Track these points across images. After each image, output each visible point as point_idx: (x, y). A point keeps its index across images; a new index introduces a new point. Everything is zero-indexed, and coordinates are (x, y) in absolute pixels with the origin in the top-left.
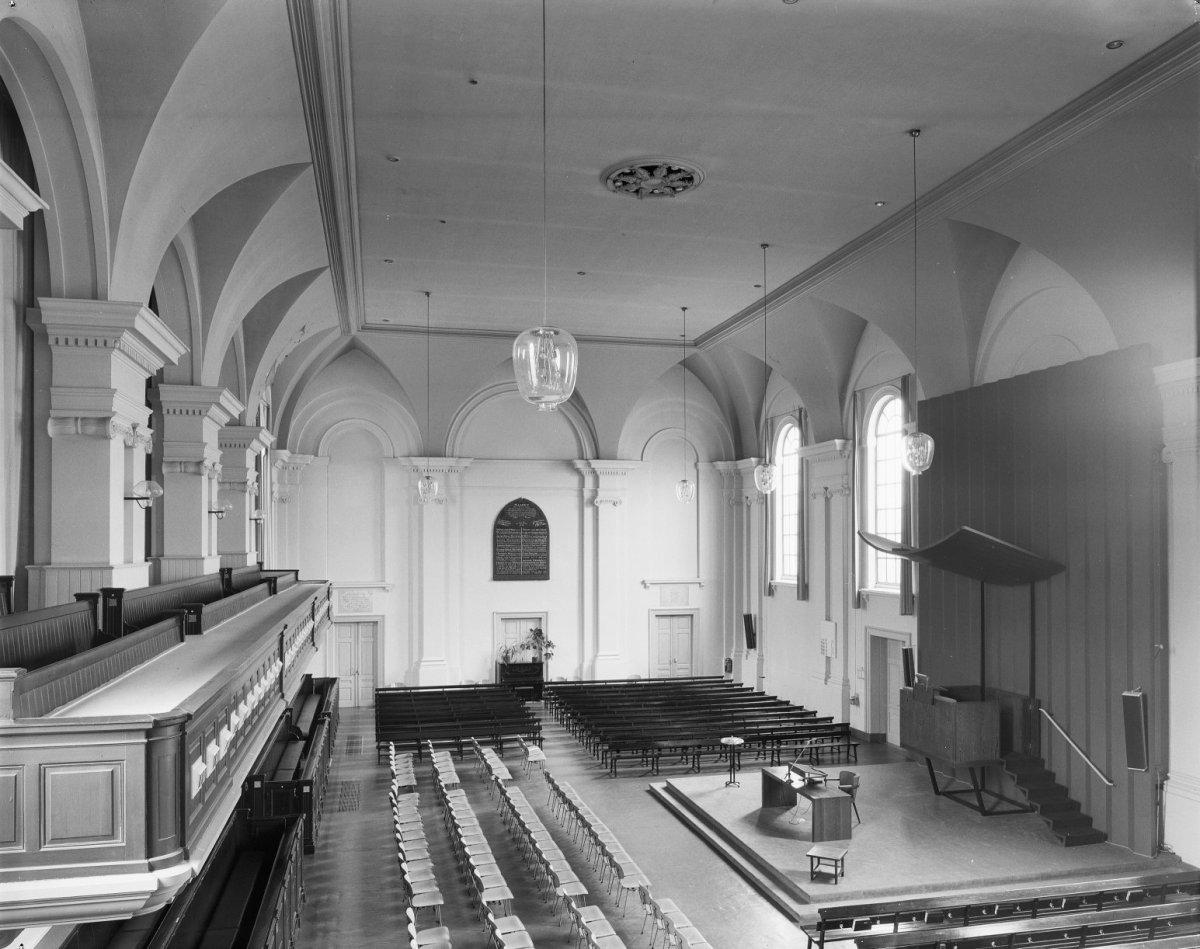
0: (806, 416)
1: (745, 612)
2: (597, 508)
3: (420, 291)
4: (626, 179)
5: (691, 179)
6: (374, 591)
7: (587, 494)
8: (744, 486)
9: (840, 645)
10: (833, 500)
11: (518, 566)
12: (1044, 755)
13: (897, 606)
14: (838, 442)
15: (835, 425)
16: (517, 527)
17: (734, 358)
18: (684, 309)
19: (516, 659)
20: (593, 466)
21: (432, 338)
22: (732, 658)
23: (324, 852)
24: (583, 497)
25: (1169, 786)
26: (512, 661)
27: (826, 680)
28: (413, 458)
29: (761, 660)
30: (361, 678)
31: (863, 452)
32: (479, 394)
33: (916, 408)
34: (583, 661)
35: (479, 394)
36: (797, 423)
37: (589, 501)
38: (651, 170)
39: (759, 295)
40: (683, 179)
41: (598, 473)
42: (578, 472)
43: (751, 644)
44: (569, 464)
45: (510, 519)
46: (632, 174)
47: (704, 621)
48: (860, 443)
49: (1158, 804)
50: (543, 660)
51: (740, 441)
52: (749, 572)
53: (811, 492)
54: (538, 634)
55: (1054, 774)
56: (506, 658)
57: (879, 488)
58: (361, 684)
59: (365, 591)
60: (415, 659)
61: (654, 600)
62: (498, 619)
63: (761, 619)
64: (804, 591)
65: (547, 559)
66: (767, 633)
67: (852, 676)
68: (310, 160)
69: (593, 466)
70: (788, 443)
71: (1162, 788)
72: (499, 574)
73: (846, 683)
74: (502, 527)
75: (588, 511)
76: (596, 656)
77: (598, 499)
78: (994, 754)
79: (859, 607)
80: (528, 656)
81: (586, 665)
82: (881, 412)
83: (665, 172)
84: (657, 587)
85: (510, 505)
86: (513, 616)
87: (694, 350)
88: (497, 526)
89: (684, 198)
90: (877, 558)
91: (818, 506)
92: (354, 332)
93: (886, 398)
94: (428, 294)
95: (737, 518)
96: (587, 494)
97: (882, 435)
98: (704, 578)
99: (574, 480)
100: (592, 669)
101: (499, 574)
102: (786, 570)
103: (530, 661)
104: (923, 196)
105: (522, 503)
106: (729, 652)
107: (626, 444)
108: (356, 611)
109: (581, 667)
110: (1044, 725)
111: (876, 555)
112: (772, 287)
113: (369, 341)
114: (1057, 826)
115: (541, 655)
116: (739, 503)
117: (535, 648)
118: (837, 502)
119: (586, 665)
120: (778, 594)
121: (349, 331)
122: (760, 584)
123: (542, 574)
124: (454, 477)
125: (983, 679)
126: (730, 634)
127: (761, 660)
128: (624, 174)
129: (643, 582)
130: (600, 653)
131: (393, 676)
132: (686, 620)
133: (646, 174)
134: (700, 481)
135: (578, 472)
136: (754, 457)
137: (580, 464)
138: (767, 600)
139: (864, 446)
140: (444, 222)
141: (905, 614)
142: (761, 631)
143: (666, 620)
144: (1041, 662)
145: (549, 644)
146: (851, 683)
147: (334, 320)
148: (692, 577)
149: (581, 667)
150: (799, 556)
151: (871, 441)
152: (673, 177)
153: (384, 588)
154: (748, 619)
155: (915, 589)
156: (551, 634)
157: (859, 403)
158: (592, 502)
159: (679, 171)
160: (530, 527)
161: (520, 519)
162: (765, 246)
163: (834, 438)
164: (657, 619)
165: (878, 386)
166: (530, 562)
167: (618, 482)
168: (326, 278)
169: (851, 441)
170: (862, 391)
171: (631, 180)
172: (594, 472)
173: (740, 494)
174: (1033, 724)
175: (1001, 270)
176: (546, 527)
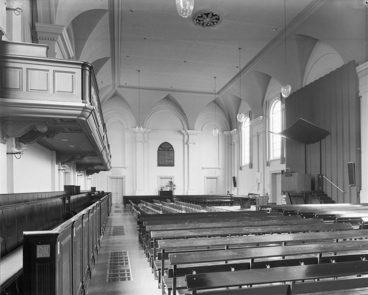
0: (251, 113)
1: (233, 176)
2: (189, 145)
3: (137, 70)
4: (199, 19)
5: (219, 19)
7: (185, 141)
8: (233, 139)
9: (262, 180)
10: (260, 136)
11: (165, 162)
12: (324, 191)
13: (280, 161)
14: (261, 117)
15: (259, 111)
16: (165, 150)
17: (228, 98)
18: (215, 78)
19: (164, 190)
20: (187, 132)
21: (141, 91)
22: (229, 191)
23: (112, 229)
25: (361, 192)
26: (163, 190)
27: (258, 190)
28: (133, 129)
29: (238, 190)
30: (118, 194)
31: (269, 119)
33: (284, 101)
36: (249, 116)
37: (186, 143)
38: (207, 15)
39: (238, 71)
40: (216, 19)
41: (189, 134)
42: (183, 134)
43: (235, 186)
44: (180, 132)
46: (202, 17)
47: (221, 179)
48: (268, 117)
49: (358, 196)
50: (173, 190)
52: (234, 164)
53: (253, 135)
54: (171, 182)
55: (327, 195)
56: (161, 189)
57: (274, 144)
58: (118, 197)
59: (119, 169)
61: (207, 173)
63: (238, 178)
64: (251, 166)
65: (174, 160)
66: (239, 182)
67: (266, 188)
68: (108, 9)
69: (187, 132)
71: (359, 193)
72: (159, 165)
73: (264, 190)
74: (160, 150)
75: (186, 146)
76: (188, 189)
77: (189, 142)
78: (309, 189)
79: (268, 166)
80: (168, 189)
81: (186, 192)
83: (211, 16)
84: (207, 169)
87: (217, 96)
88: (159, 150)
89: (217, 27)
91: (255, 139)
92: (116, 88)
93: (277, 101)
94: (139, 71)
95: (230, 145)
96: (185, 141)
98: (220, 167)
99: (182, 137)
101: (159, 165)
102: (246, 160)
103: (169, 190)
104: (288, 25)
105: (166, 143)
106: (228, 188)
107: (196, 126)
108: (117, 175)
109: (184, 193)
110: (324, 180)
112: (242, 67)
113: (121, 91)
115: (172, 188)
116: (231, 144)
117: (170, 186)
118: (261, 136)
119: (186, 189)
121: (115, 88)
122: (237, 166)
123: (172, 165)
124: (146, 135)
125: (305, 147)
126: (228, 184)
127: (238, 190)
128: (199, 17)
129: (202, 168)
130: (190, 188)
131: (128, 193)
132: (215, 180)
133: (205, 16)
135: (183, 134)
136: (235, 128)
137: (183, 132)
138: (240, 171)
139: (269, 117)
140: (145, 39)
141: (282, 163)
142: (238, 181)
143: (209, 179)
144: (323, 160)
145: (174, 185)
146: (266, 190)
147: (110, 82)
151: (271, 116)
152: (214, 18)
153: (125, 168)
154: (234, 178)
155: (285, 156)
156: (175, 183)
157: (268, 105)
158: (187, 143)
159: (216, 15)
160: (168, 150)
161: (166, 148)
164: (206, 179)
165: (273, 98)
166: (168, 161)
167: (194, 136)
168: (109, 62)
169: (265, 117)
170: (269, 101)
171: (201, 19)
172: (188, 134)
173: (231, 142)
174: (321, 181)
175: (313, 47)
176: (173, 150)
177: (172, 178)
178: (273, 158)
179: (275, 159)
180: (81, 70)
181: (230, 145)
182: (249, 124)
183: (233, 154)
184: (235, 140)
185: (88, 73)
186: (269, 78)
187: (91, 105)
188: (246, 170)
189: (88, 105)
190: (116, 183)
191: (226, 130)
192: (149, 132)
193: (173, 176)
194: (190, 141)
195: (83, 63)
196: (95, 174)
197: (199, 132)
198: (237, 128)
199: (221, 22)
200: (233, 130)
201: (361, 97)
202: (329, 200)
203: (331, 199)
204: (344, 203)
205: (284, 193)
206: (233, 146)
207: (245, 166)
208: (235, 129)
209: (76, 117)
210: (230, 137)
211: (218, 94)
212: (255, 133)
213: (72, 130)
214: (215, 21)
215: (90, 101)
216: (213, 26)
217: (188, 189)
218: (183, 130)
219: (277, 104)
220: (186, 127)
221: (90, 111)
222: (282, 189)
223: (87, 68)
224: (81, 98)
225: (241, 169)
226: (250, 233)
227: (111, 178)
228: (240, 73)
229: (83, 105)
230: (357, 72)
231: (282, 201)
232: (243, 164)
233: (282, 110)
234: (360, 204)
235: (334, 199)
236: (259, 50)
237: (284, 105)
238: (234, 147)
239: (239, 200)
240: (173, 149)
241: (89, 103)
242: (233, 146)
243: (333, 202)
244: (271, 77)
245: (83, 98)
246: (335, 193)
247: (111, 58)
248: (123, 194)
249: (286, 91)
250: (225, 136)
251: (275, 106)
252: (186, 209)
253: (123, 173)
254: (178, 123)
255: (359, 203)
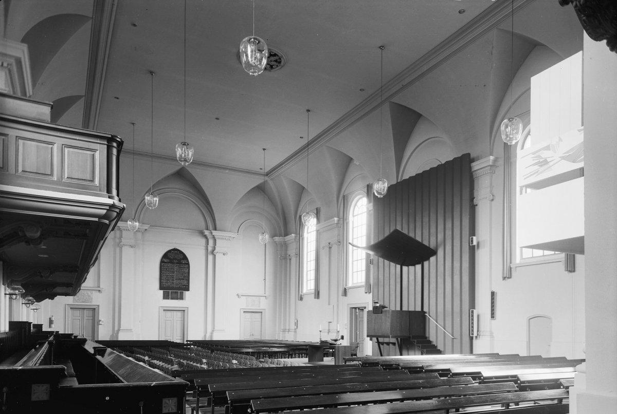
2: (215, 255)
5: (280, 62)
6: (94, 292)
7: (210, 249)
11: (173, 283)
12: (427, 335)
13: (363, 289)
15: (335, 211)
18: (264, 149)
24: (207, 249)
32: (160, 189)
34: (206, 333)
35: (160, 189)
39: (304, 142)
40: (276, 61)
42: (205, 237)
44: (202, 233)
45: (170, 259)
51: (284, 227)
60: (116, 329)
61: (243, 303)
62: (162, 310)
64: (317, 294)
70: (311, 225)
75: (210, 257)
76: (213, 331)
81: (209, 331)
82: (356, 205)
84: (245, 297)
85: (169, 251)
86: (168, 309)
87: (266, 178)
88: (162, 262)
90: (353, 250)
95: (285, 259)
96: (210, 249)
97: (356, 216)
98: (267, 294)
99: (203, 241)
100: (211, 336)
102: (309, 285)
108: (84, 302)
109: (205, 336)
111: (353, 248)
114: (423, 348)
116: (285, 258)
118: (335, 248)
119: (209, 331)
120: (305, 298)
129: (238, 295)
132: (260, 314)
134: (267, 248)
135: (205, 237)
137: (207, 233)
143: (249, 315)
148: (261, 293)
149: (205, 336)
150: (316, 270)
151: (351, 218)
152: (273, 58)
153: (99, 291)
157: (345, 201)
160: (179, 263)
161: (175, 259)
162: (308, 111)
163: (333, 218)
166: (178, 282)
172: (214, 237)
173: (286, 254)
176: (188, 264)
177: (184, 311)
178: (353, 283)
179: (355, 285)
180: (106, 146)
181: (285, 259)
182: (315, 227)
183: (288, 277)
184: (292, 251)
185: (115, 151)
186: (348, 161)
187: (120, 200)
188: (310, 300)
189: (115, 201)
190: (80, 318)
191: (283, 234)
192: (146, 230)
193: (188, 308)
194: (217, 249)
195: (110, 136)
196: (47, 300)
197: (233, 236)
198: (296, 234)
199: (282, 67)
200: (289, 236)
201: (477, 205)
202: (431, 349)
203: (436, 347)
204: (453, 353)
205: (370, 336)
206: (288, 260)
207: (307, 294)
208: (293, 235)
209: (96, 219)
210: (285, 246)
211: (267, 175)
212: (324, 243)
213: (70, 235)
214: (274, 63)
215: (118, 195)
216: (270, 71)
217: (213, 331)
218: (207, 231)
219: (361, 200)
220: (211, 227)
221: (118, 210)
222: (367, 333)
223: (115, 144)
224: (106, 191)
225: (301, 299)
226: (286, 408)
227: (71, 308)
228: (308, 146)
229: (110, 202)
230: (472, 170)
231: (368, 349)
232: (305, 291)
233: (369, 212)
234: (475, 355)
235: (440, 347)
236: (337, 117)
237: (372, 204)
238: (290, 262)
239: (306, 350)
240: (188, 261)
241: (116, 198)
242: (288, 260)
243: (439, 352)
244: (352, 159)
245: (109, 191)
246: (441, 338)
247: (84, 97)
248: (94, 336)
249: (381, 187)
250: (276, 244)
251: (358, 204)
252: (180, 364)
253: (97, 299)
254: (197, 218)
255: (471, 352)
